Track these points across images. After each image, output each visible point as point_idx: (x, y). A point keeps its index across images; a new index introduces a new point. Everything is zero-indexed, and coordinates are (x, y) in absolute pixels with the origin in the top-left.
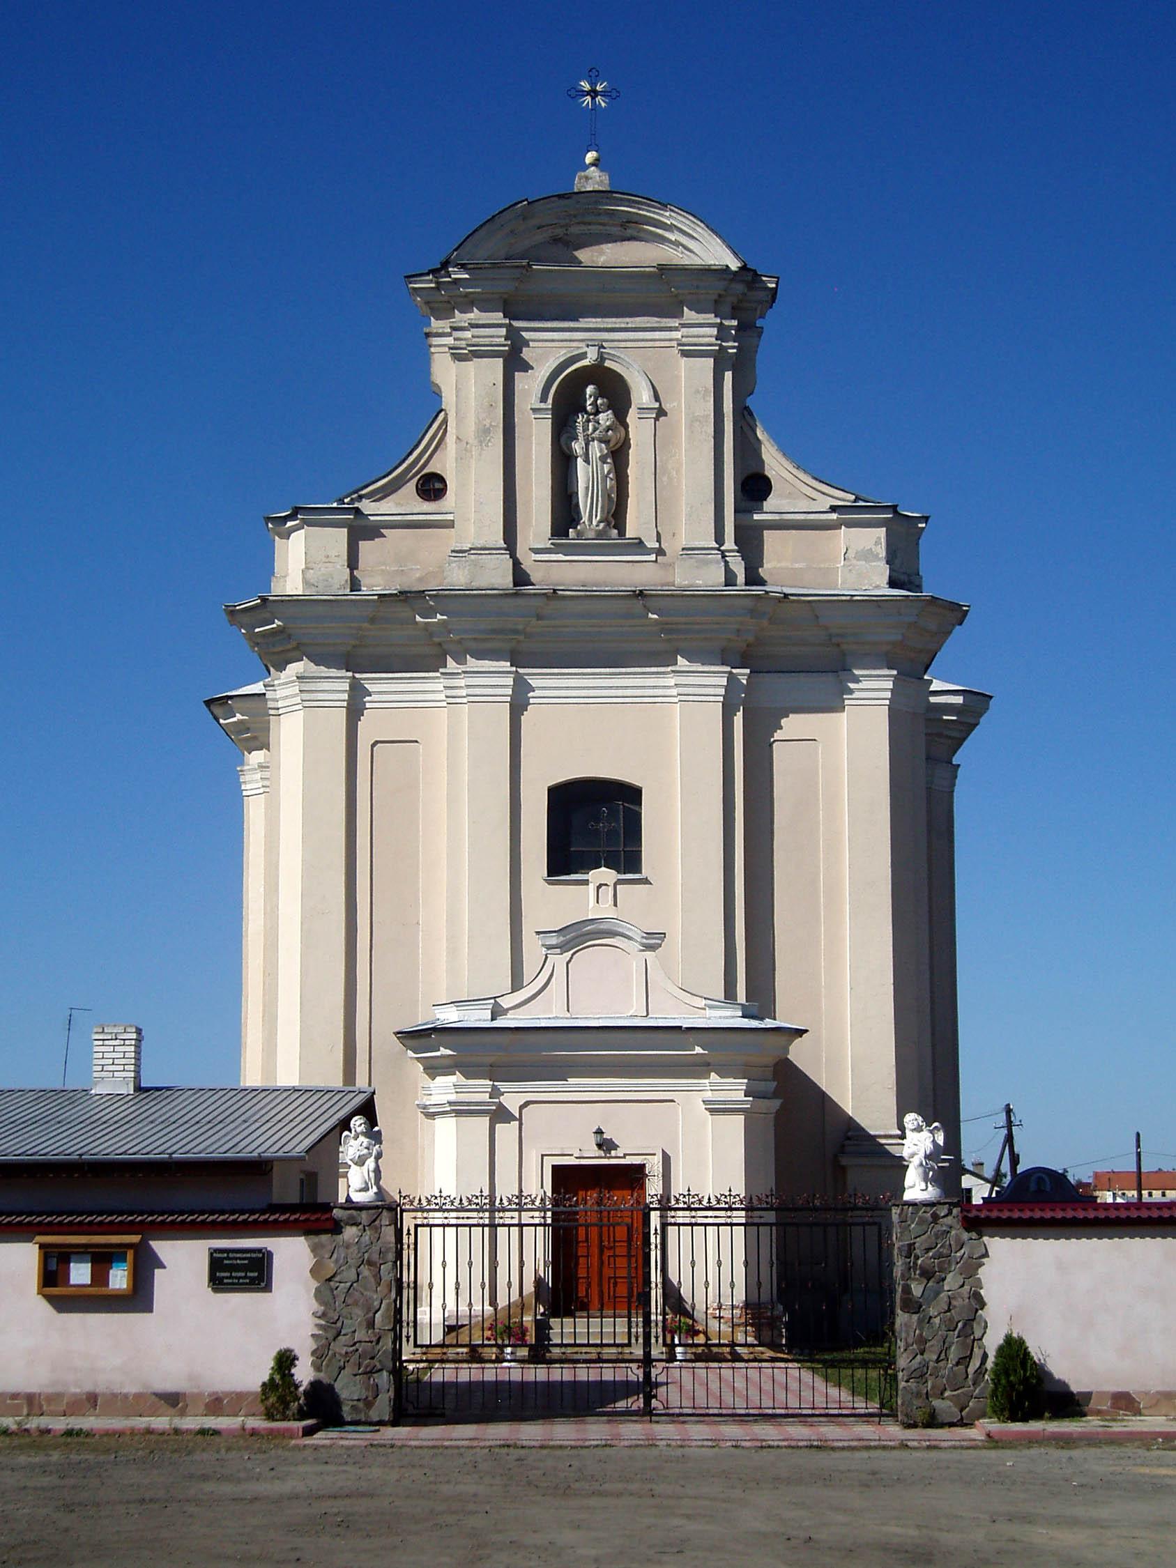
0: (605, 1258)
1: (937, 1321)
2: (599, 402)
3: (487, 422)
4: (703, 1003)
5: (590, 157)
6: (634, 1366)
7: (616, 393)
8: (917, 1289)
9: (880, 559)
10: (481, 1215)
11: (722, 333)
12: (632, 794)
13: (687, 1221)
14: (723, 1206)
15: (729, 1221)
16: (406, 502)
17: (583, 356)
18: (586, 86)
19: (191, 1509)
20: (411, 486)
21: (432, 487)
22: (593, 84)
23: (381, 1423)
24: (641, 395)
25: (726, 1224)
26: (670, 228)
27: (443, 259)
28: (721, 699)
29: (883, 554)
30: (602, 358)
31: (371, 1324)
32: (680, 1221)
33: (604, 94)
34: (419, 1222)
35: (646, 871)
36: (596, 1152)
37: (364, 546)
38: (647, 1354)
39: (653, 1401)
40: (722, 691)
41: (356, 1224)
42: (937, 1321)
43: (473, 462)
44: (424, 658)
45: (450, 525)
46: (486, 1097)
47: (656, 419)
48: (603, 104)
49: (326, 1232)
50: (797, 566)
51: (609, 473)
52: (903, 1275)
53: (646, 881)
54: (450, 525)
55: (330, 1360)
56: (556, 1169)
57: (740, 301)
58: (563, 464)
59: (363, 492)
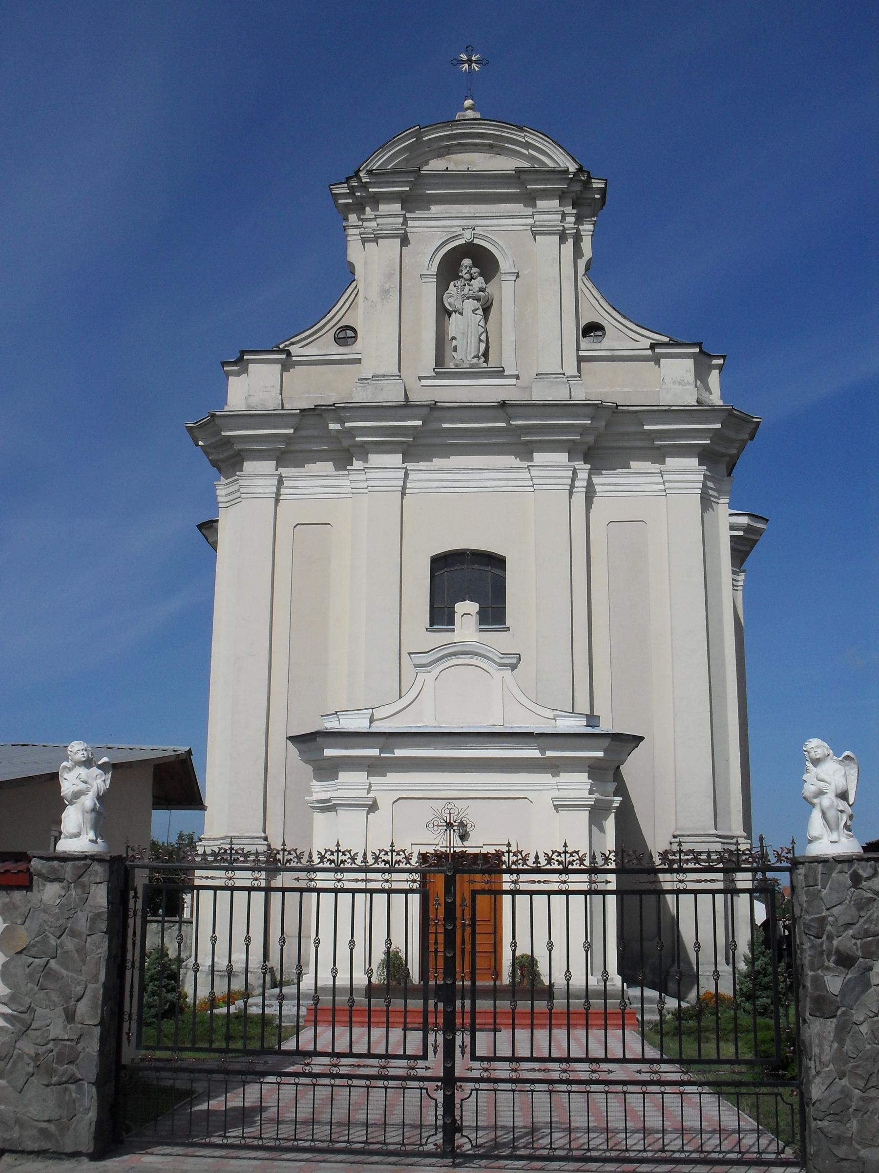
1: (864, 1029)
3: (387, 286)
4: (550, 714)
5: (468, 103)
6: (431, 1085)
7: (485, 262)
8: (834, 983)
9: (688, 383)
10: (256, 874)
12: (497, 562)
13: (330, 885)
14: (556, 866)
15: (564, 887)
18: (464, 57)
21: (346, 335)
22: (469, 56)
23: (75, 1155)
24: (505, 265)
25: (559, 892)
26: (528, 145)
28: (584, 490)
31: (70, 1016)
32: (320, 885)
33: (476, 62)
34: (478, 886)
35: (508, 623)
38: (449, 1070)
39: (458, 1135)
41: (60, 880)
42: (864, 1029)
44: (345, 453)
45: (358, 361)
48: (477, 69)
49: (19, 888)
50: (625, 390)
52: (812, 963)
53: (508, 629)
54: (358, 361)
55: (15, 1064)
57: (578, 198)
58: (444, 312)
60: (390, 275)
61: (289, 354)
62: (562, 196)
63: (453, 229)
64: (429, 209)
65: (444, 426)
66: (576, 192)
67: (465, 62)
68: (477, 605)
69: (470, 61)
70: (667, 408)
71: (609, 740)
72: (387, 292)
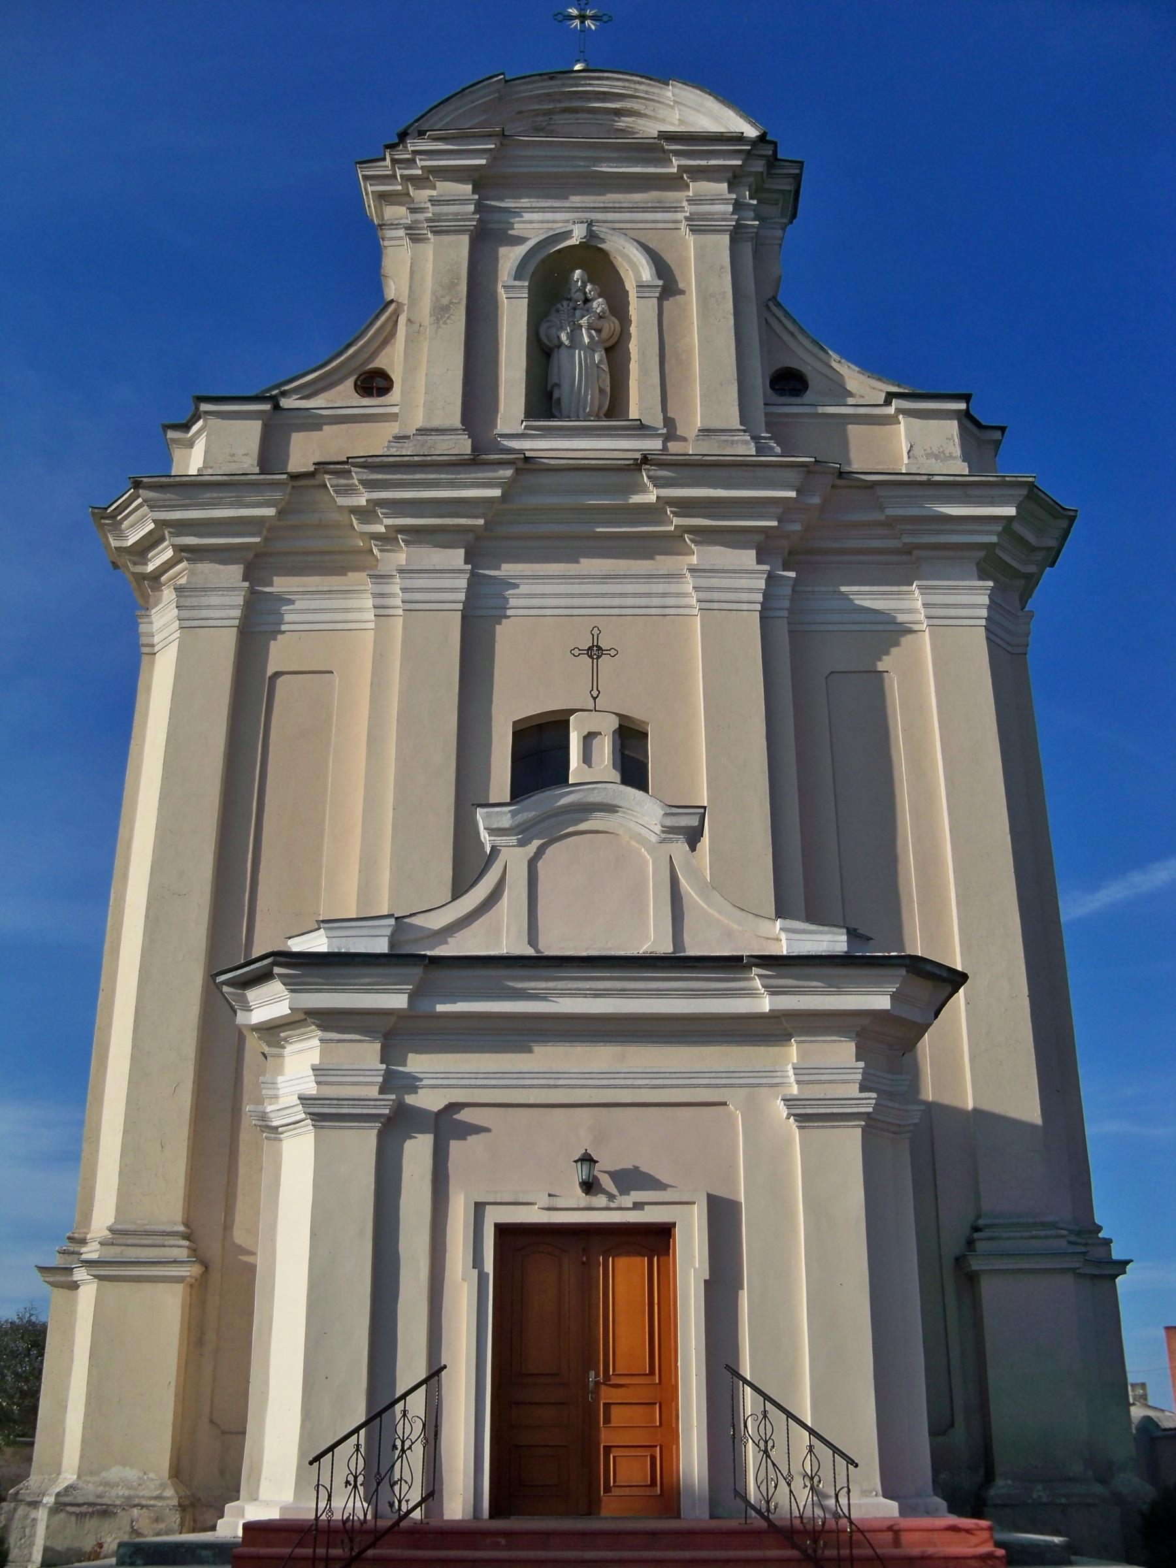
0: (776, 196)
2: (589, 287)
3: (445, 301)
9: (955, 458)
11: (738, 206)
16: (344, 396)
17: (568, 234)
18: (574, 12)
19: (772, 1505)
20: (350, 383)
21: (375, 383)
24: (636, 270)
27: (401, 129)
28: (759, 607)
29: (958, 452)
30: (591, 235)
33: (593, 18)
36: (578, 1197)
37: (454, 1146)
40: (760, 597)
43: (426, 344)
46: (374, 1092)
47: (661, 299)
48: (593, 27)
51: (600, 361)
56: (504, 1231)
59: (287, 388)
60: (453, 286)
61: (277, 407)
62: (734, 179)
63: (550, 226)
64: (447, 943)
65: (441, 1008)
66: (756, 174)
67: (576, 17)
68: (410, 1055)
69: (582, 18)
70: (925, 478)
71: (903, 972)
72: (445, 309)
